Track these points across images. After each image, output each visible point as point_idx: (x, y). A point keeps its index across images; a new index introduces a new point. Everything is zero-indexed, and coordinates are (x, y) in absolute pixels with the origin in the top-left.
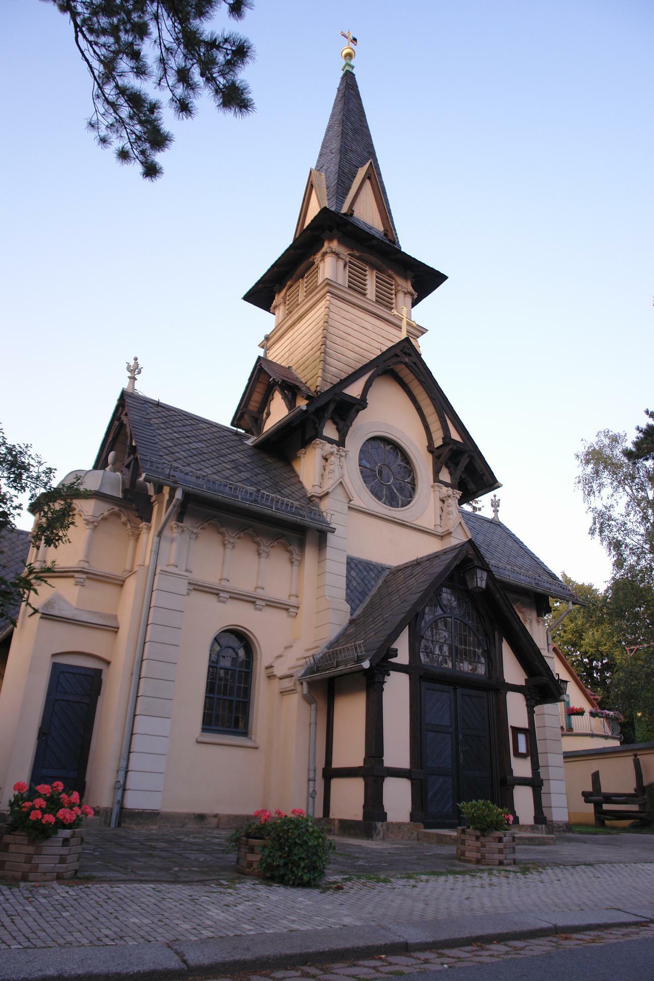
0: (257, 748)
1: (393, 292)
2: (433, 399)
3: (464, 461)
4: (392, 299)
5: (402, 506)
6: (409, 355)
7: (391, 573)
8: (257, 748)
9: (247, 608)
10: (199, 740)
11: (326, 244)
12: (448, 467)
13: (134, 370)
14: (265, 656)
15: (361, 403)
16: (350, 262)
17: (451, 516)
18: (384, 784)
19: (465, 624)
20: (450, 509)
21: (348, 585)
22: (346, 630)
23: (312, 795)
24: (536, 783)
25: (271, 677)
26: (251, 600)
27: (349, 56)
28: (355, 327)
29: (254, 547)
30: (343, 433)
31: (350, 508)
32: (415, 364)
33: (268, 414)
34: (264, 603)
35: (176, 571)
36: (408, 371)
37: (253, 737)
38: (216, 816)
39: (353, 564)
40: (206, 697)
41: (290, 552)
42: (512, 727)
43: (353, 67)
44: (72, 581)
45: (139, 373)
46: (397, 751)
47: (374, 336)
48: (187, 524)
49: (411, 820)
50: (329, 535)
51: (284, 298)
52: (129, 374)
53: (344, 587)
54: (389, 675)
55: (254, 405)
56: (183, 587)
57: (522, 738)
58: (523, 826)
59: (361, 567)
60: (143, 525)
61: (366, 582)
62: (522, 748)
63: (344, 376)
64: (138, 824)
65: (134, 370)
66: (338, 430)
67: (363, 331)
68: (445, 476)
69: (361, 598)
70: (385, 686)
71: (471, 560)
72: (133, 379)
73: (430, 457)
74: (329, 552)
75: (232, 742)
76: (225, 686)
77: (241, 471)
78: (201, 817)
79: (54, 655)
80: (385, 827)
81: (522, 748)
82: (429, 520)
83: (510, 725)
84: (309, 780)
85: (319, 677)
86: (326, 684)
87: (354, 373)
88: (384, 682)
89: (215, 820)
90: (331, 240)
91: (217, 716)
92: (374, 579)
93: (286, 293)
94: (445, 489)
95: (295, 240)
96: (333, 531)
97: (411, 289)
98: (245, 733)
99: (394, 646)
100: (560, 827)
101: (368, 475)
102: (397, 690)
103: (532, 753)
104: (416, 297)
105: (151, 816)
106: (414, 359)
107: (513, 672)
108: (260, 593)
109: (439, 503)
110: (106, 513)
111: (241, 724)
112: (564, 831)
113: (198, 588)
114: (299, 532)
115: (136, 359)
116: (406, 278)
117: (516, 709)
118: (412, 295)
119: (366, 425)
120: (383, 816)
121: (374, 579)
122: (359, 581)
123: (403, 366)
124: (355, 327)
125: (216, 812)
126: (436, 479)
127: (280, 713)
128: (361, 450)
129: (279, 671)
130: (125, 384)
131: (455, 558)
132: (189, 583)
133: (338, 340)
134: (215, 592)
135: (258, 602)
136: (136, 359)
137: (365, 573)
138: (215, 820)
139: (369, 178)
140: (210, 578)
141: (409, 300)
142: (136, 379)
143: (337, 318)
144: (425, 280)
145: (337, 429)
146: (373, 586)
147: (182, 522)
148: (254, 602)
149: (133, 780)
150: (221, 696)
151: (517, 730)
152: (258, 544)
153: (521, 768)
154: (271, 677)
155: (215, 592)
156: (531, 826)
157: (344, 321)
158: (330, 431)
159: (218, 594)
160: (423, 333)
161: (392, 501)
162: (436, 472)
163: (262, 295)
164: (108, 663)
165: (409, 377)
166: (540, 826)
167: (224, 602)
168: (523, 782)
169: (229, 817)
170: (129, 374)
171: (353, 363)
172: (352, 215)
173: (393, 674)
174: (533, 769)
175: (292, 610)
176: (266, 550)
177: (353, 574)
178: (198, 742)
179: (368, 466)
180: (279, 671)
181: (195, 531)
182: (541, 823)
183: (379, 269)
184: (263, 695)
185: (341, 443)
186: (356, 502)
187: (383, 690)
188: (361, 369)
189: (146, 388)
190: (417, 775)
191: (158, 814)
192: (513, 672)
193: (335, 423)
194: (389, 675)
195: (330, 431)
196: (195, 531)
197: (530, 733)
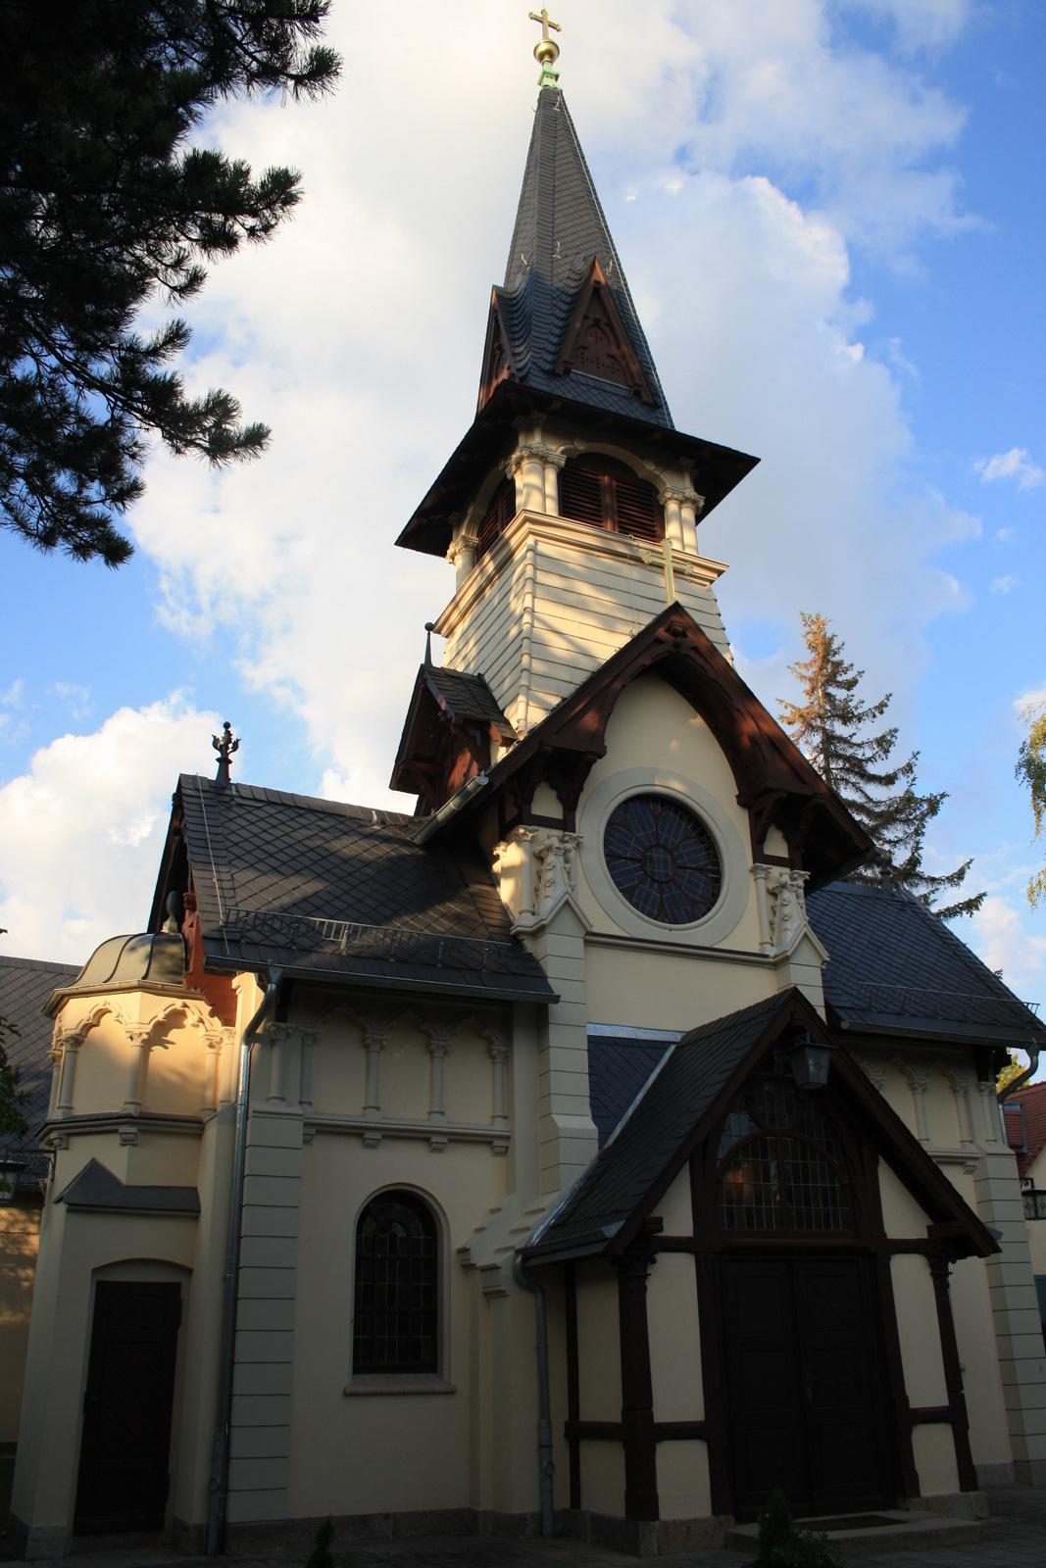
11: (522, 441)
12: (780, 827)
14: (459, 1231)
17: (788, 925)
20: (786, 910)
23: (547, 1473)
24: (954, 1415)
25: (468, 1267)
27: (549, 55)
30: (570, 804)
34: (444, 1139)
35: (281, 1108)
39: (601, 1048)
43: (557, 77)
44: (116, 1139)
45: (235, 747)
46: (679, 1387)
50: (552, 1007)
52: (218, 755)
56: (296, 1130)
68: (777, 846)
72: (224, 762)
74: (556, 1036)
75: (408, 1388)
79: (95, 1271)
82: (747, 936)
84: (541, 1446)
86: (555, 1271)
90: (529, 431)
94: (776, 871)
95: (479, 417)
96: (556, 999)
97: (691, 492)
99: (656, 1214)
104: (702, 504)
107: (900, 1216)
113: (323, 1130)
116: (679, 470)
118: (694, 502)
123: (676, 660)
126: (759, 856)
127: (485, 1335)
132: (306, 1124)
134: (355, 1132)
136: (227, 726)
141: (688, 514)
144: (718, 471)
145: (560, 798)
147: (285, 1020)
149: (240, 1475)
155: (355, 1132)
158: (546, 804)
162: (758, 841)
163: (426, 532)
164: (189, 1271)
167: (373, 1147)
168: (931, 1416)
170: (218, 755)
175: (497, 1143)
181: (310, 1031)
184: (456, 1297)
185: (567, 824)
186: (602, 925)
190: (722, 1429)
192: (900, 1216)
194: (654, 1262)
195: (546, 804)
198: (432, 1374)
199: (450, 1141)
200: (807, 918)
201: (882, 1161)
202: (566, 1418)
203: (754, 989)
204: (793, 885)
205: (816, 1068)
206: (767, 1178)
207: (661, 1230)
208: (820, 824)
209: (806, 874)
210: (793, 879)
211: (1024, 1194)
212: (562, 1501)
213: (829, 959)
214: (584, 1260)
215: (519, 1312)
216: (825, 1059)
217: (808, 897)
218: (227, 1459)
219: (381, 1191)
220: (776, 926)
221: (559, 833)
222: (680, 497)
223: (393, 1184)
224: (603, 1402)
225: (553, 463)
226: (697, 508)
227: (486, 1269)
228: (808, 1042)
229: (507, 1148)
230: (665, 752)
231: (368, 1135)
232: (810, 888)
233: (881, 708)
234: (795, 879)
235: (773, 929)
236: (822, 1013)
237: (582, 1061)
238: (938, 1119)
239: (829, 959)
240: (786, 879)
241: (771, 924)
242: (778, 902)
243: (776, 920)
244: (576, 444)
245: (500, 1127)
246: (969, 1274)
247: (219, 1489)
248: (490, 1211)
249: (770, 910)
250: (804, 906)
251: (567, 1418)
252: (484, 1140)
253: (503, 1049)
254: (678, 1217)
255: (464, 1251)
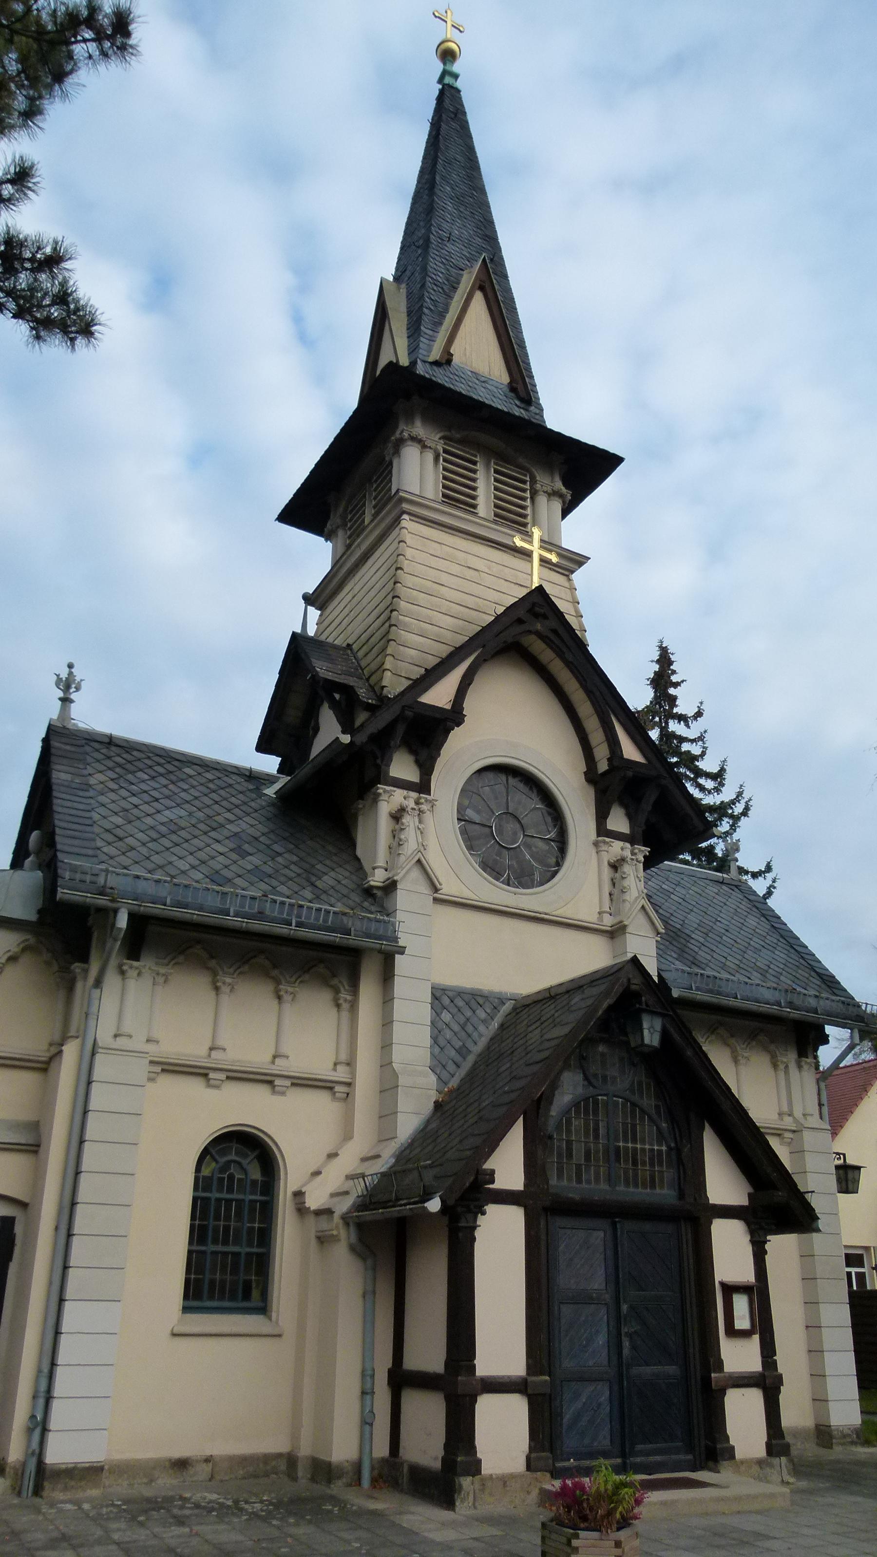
0: (280, 1336)
1: (528, 495)
2: (589, 693)
3: (651, 796)
4: (524, 508)
5: (542, 884)
6: (545, 617)
7: (514, 1009)
8: (280, 1336)
9: (259, 1094)
10: (175, 1331)
11: (402, 426)
13: (67, 686)
14: (292, 1176)
15: (454, 716)
16: (445, 451)
18: (478, 1407)
19: (634, 1105)
21: (435, 1039)
22: (428, 1122)
23: (367, 1422)
24: (768, 1383)
25: (301, 1210)
26: (266, 1080)
28: (455, 569)
29: (271, 987)
30: (426, 768)
31: (436, 900)
32: (555, 631)
33: (317, 730)
34: (288, 1083)
36: (543, 646)
37: (274, 1315)
38: (207, 1460)
39: (442, 997)
40: (190, 1253)
41: (337, 991)
42: (723, 1285)
45: (78, 689)
46: (501, 1342)
47: (489, 580)
48: (147, 963)
49: (529, 1468)
51: (344, 517)
52: (61, 694)
53: (428, 1042)
54: (484, 1213)
55: (292, 715)
57: (741, 1304)
58: (742, 1462)
59: (461, 1003)
60: (77, 967)
61: (470, 1028)
62: (742, 1322)
63: (432, 662)
64: (66, 1489)
65: (67, 686)
66: (419, 764)
67: (469, 574)
68: (618, 822)
69: (458, 1058)
70: (478, 1233)
71: (637, 995)
72: (66, 701)
73: (591, 792)
76: (227, 1229)
77: (244, 854)
78: (181, 1464)
80: (477, 1486)
81: (742, 1322)
83: (718, 1278)
85: (368, 1218)
87: (438, 665)
88: (474, 1228)
89: (208, 1468)
91: (212, 1282)
92: (484, 1021)
93: (345, 510)
94: (617, 845)
96: (402, 951)
97: (559, 485)
98: (263, 1309)
99: (488, 1165)
100: (844, 1436)
101: (473, 833)
102: (501, 1241)
103: (763, 1326)
105: (91, 1473)
106: (553, 623)
107: (723, 1183)
108: (281, 1066)
109: (607, 872)
110: (15, 950)
111: (255, 1293)
112: (853, 1443)
114: (339, 959)
115: (70, 666)
117: (730, 1251)
118: (561, 496)
119: (462, 753)
120: (475, 1468)
121: (484, 1021)
122: (456, 1028)
123: (538, 638)
124: (455, 569)
125: (208, 1453)
126: (602, 831)
128: (463, 790)
129: (313, 1202)
130: (53, 711)
131: (607, 994)
133: (422, 598)
134: (200, 1073)
135: (277, 1082)
136: (70, 666)
137: (469, 1013)
138: (208, 1468)
139: (482, 288)
140: (190, 1047)
142: (72, 701)
143: (420, 557)
144: (583, 468)
145: (417, 762)
146: (481, 1035)
148: (270, 1083)
150: (220, 1248)
151: (729, 1290)
152: (278, 982)
153: (739, 1356)
154: (301, 1210)
156: (760, 1462)
157: (434, 562)
158: (402, 767)
159: (206, 1075)
160: (580, 564)
161: (523, 878)
162: (601, 816)
165: (546, 655)
166: (775, 1461)
167: (217, 1087)
168: (743, 1381)
169: (231, 1459)
170: (61, 694)
171: (448, 637)
172: (449, 362)
173: (490, 1208)
174: (763, 1356)
175: (338, 1088)
176: (290, 989)
177: (446, 1016)
178: (174, 1335)
179: (477, 818)
180: (313, 1202)
182: (779, 1455)
183: (502, 458)
184: (289, 1239)
185: (423, 787)
187: (474, 1239)
188: (451, 655)
189: (91, 715)
191: (102, 1469)
192: (723, 1183)
193: (413, 751)
194: (484, 1213)
195: (402, 767)
196: (162, 970)
197: (759, 1292)
198: (262, 1316)
199: (293, 1084)
200: (645, 891)
201: (707, 1125)
202: (389, 1364)
203: (587, 957)
204: (632, 859)
205: (651, 1033)
206: (597, 1136)
207: (493, 1182)
208: (660, 799)
209: (646, 850)
210: (633, 854)
211: (837, 1167)
212: (381, 1449)
213: (663, 931)
214: (406, 1224)
215: (345, 1271)
216: (658, 1023)
217: (648, 871)
218: (49, 1398)
219: (217, 1134)
220: (614, 897)
221: (414, 795)
222: (549, 490)
223: (227, 1127)
224: (428, 1352)
225: (430, 447)
226: (564, 503)
227: (318, 1213)
228: (644, 1007)
229: (348, 1094)
230: (507, 721)
231: (212, 1075)
232: (649, 863)
233: (699, 714)
234: (635, 854)
235: (611, 900)
236: (656, 979)
237: (425, 1012)
238: (759, 1087)
239: (663, 931)
240: (627, 853)
241: (610, 894)
242: (617, 875)
243: (616, 891)
244: (453, 432)
245: (342, 1074)
246: (782, 1247)
247: (40, 1426)
248: (323, 1157)
249: (610, 882)
250: (642, 879)
251: (390, 1365)
252: (326, 1086)
253: (349, 998)
254: (508, 1166)
255: (299, 1195)
